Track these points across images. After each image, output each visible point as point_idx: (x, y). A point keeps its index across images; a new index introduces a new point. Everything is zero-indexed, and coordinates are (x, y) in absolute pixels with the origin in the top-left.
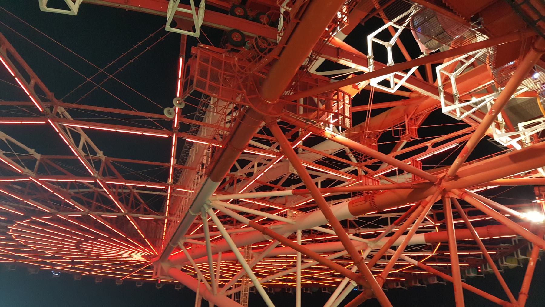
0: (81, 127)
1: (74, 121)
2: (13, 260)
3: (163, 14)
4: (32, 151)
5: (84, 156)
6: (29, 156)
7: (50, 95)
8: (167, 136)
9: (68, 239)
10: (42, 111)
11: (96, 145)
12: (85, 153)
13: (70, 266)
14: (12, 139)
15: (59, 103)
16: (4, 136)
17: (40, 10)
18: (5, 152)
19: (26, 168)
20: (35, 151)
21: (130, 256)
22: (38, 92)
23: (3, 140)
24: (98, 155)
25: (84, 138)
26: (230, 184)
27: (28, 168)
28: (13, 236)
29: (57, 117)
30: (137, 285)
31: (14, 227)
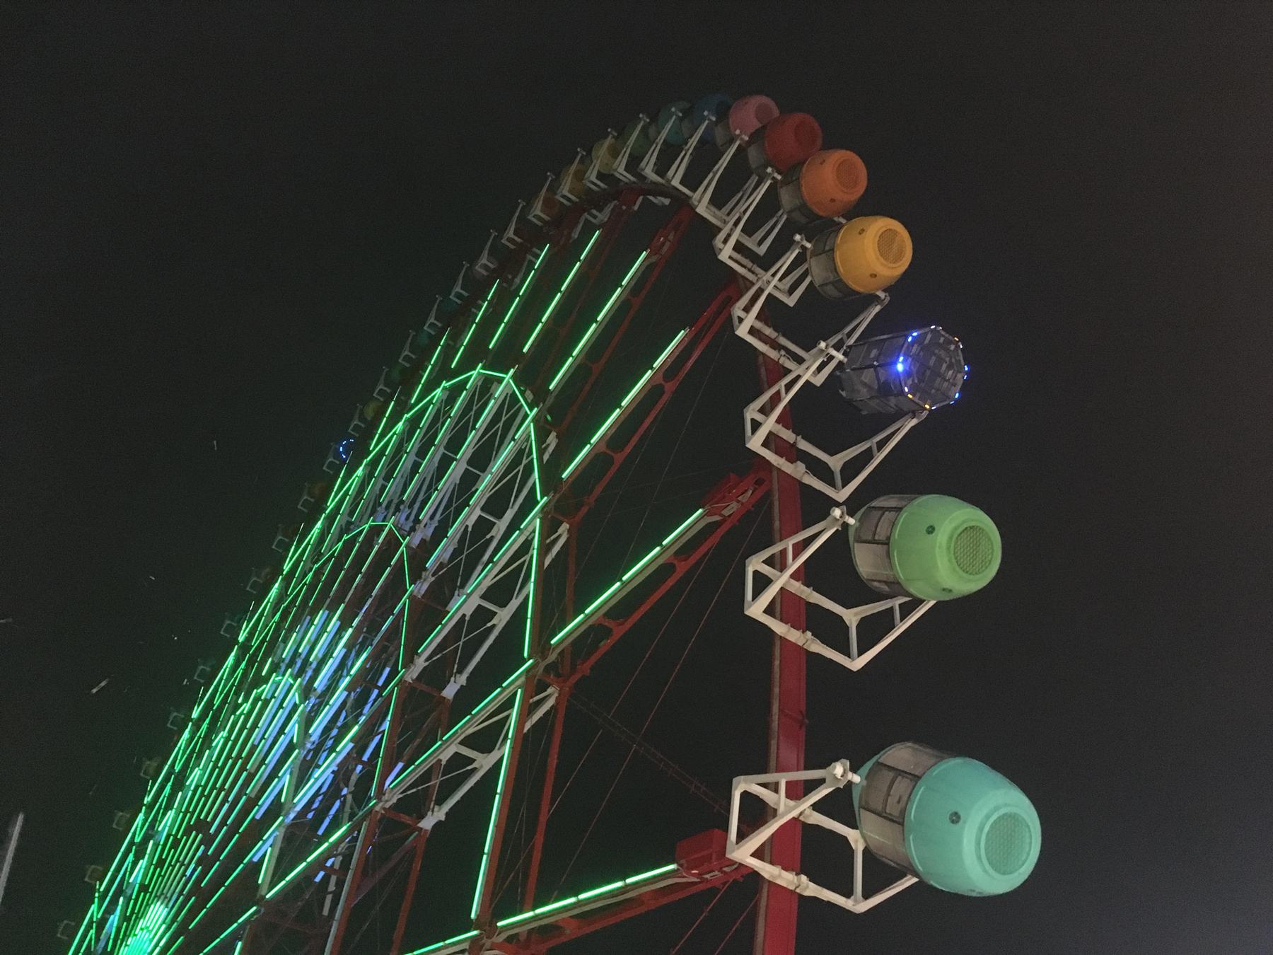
0: (529, 592)
1: (528, 706)
2: (241, 638)
3: (773, 763)
4: (462, 679)
5: (440, 757)
6: (429, 808)
7: (585, 668)
8: (473, 916)
9: (225, 835)
10: (551, 645)
11: (482, 659)
12: (447, 761)
13: (177, 768)
14: (475, 782)
15: (567, 689)
16: (482, 767)
17: (747, 558)
18: (467, 618)
19: (427, 663)
20: (462, 686)
21: (142, 929)
22: (593, 633)
23: (492, 620)
24: (436, 808)
25: (484, 762)
26: (448, 414)
27: (425, 668)
28: (280, 678)
29: (535, 686)
30: (65, 922)
31: (294, 696)
